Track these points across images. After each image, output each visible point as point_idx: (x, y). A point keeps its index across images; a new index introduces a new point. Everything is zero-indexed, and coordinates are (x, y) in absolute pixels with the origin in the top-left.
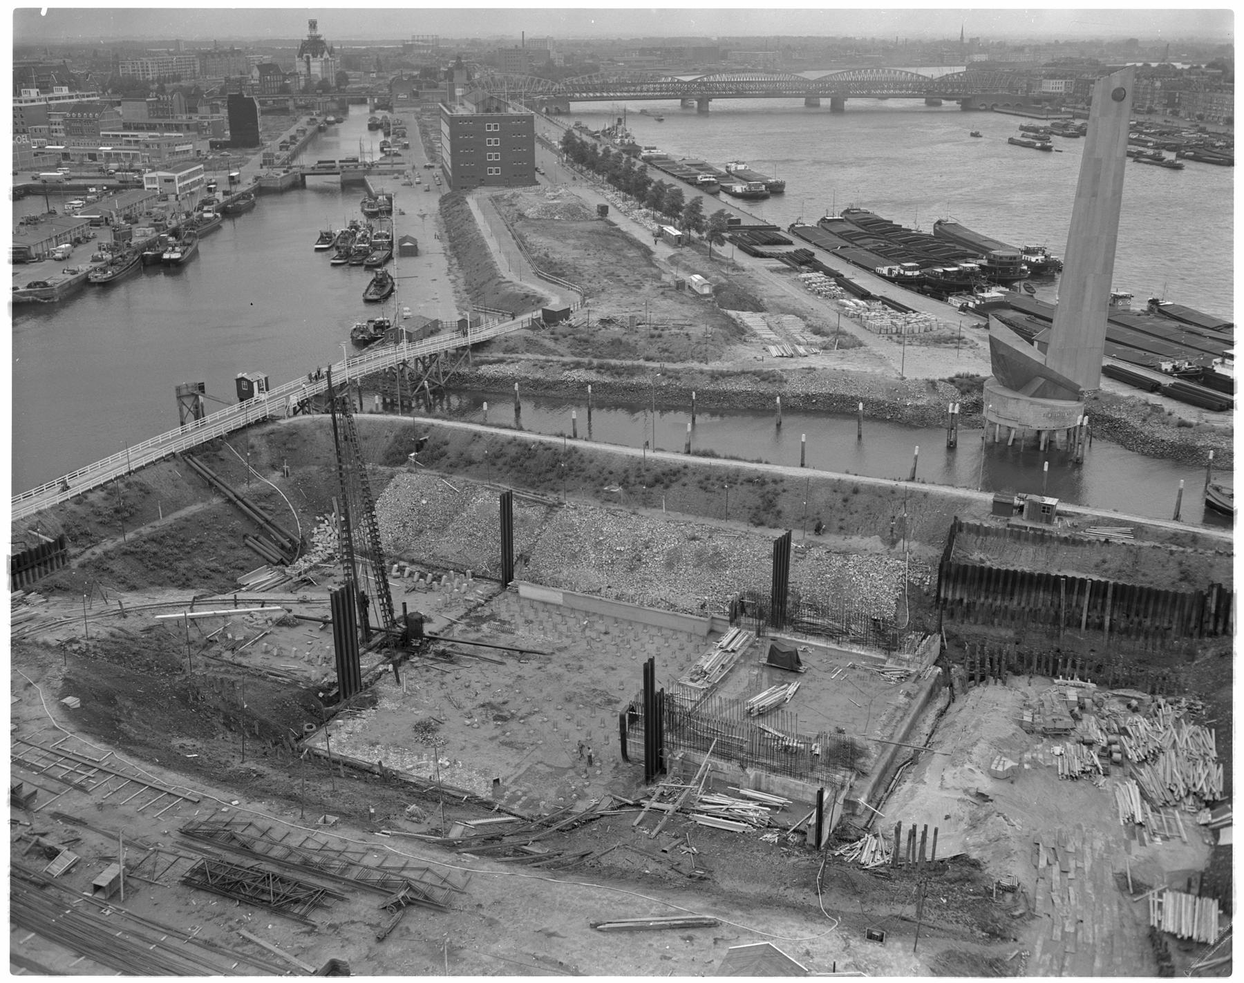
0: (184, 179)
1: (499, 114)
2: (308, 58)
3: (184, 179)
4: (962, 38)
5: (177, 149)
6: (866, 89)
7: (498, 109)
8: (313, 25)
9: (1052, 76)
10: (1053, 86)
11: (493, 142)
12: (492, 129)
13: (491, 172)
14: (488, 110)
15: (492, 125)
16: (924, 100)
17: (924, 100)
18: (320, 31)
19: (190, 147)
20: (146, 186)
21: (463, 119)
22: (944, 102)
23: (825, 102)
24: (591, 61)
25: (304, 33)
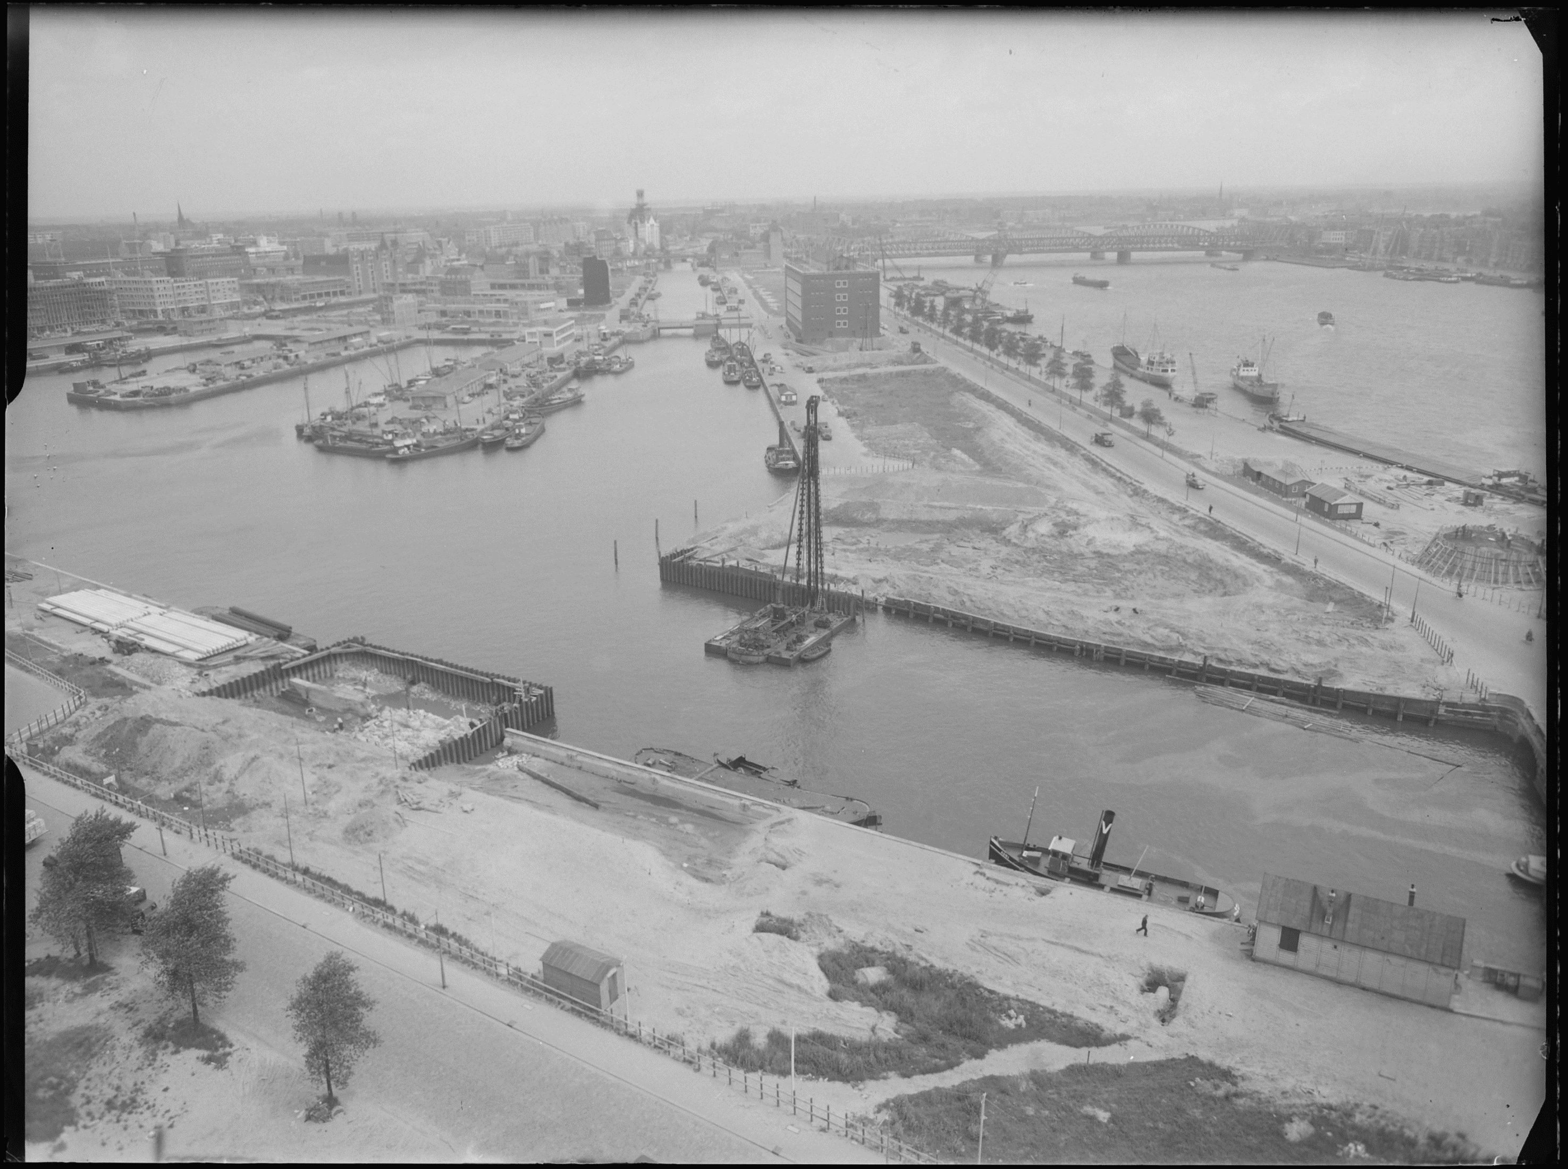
0: (562, 331)
1: (848, 272)
2: (636, 224)
3: (562, 331)
4: (1221, 194)
5: (542, 306)
6: (1143, 242)
7: (847, 267)
8: (640, 194)
9: (1333, 228)
10: (1336, 237)
11: (841, 297)
12: (842, 286)
13: (839, 324)
14: (838, 268)
15: (841, 282)
16: (1204, 252)
17: (1204, 252)
18: (647, 199)
19: (552, 304)
20: (528, 340)
21: (814, 277)
22: (1224, 253)
23: (1112, 256)
24: (876, 222)
25: (631, 201)
